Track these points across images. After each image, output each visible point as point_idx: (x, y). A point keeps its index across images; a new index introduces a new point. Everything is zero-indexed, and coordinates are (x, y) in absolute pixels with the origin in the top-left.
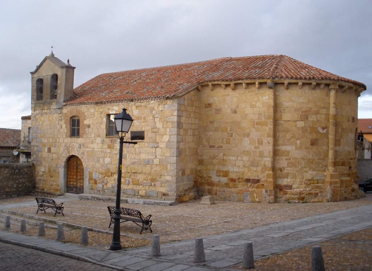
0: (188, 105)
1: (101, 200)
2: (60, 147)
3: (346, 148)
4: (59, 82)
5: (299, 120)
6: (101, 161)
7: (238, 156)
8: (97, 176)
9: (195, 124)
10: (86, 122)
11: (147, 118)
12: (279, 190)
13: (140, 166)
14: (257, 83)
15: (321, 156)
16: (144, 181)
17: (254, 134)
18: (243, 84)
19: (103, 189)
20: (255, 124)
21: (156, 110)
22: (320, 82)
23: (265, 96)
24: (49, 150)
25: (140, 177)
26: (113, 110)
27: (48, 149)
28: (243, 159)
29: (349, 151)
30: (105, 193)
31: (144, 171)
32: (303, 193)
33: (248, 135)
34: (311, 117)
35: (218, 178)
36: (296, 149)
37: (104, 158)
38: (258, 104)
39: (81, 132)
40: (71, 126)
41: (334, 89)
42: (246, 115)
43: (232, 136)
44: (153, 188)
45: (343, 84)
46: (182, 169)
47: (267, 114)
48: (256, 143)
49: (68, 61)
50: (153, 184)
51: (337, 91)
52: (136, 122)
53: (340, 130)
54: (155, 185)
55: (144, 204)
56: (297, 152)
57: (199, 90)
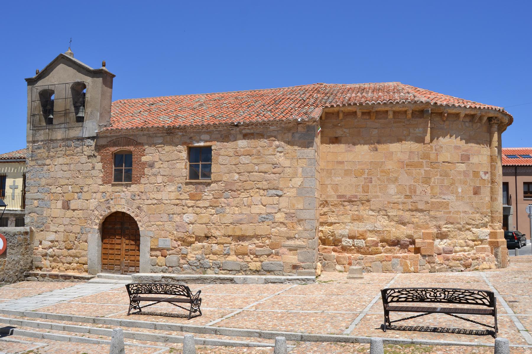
24: (66, 206)
28: (389, 214)
31: (258, 233)
35: (351, 241)
39: (135, 173)
42: (392, 153)
55: (266, 283)
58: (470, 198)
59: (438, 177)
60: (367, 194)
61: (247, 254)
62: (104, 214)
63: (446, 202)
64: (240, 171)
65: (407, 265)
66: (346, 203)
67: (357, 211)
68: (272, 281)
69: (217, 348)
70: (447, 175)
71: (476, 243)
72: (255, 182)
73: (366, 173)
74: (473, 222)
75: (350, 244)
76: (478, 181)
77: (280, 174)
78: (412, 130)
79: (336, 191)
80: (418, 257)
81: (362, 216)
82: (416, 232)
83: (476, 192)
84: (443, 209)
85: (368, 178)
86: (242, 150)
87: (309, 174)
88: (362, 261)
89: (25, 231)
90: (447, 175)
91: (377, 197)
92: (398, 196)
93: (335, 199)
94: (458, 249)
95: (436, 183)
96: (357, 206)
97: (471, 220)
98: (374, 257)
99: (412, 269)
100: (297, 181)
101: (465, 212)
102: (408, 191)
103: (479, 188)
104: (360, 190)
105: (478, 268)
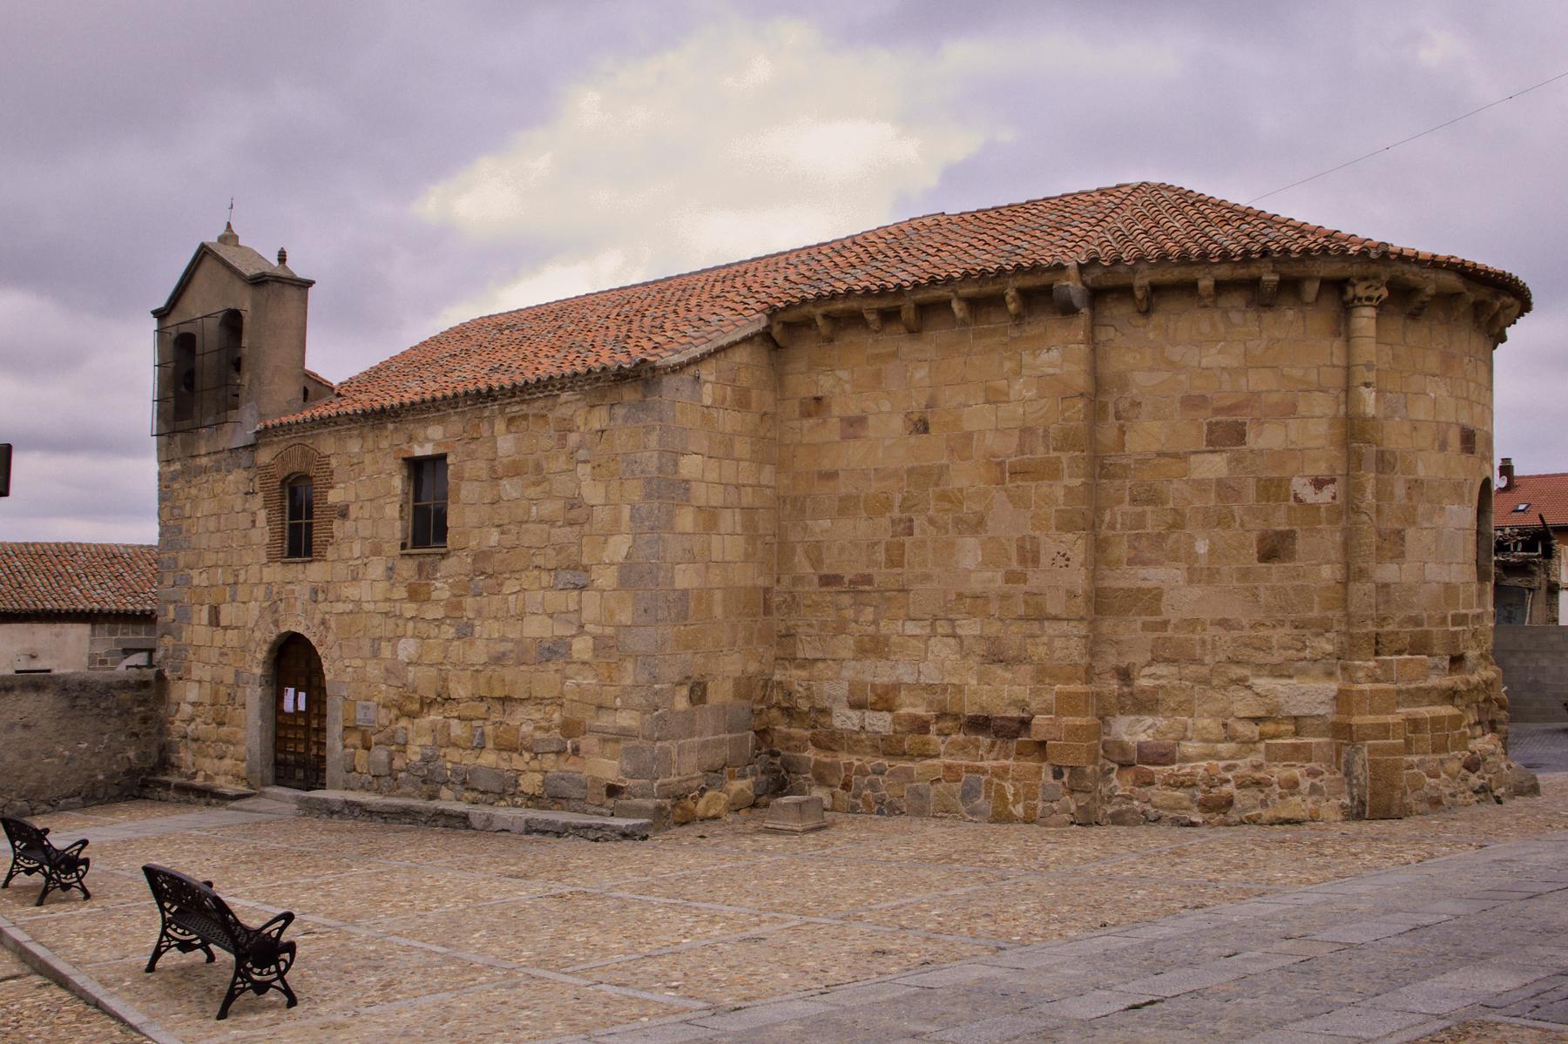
0: (720, 403)
1: (375, 817)
2: (250, 601)
3: (1433, 571)
4: (245, 341)
5: (1204, 448)
6: (386, 651)
7: (935, 619)
9: (760, 485)
10: (334, 497)
11: (548, 464)
12: (1116, 767)
13: (523, 668)
14: (1011, 293)
15: (1311, 609)
16: (539, 735)
17: (1007, 522)
18: (955, 306)
19: (391, 768)
20: (1007, 474)
21: (582, 429)
22: (1295, 271)
23: (1049, 350)
24: (215, 620)
25: (525, 721)
26: (427, 440)
27: (210, 612)
28: (959, 631)
29: (1447, 586)
30: (399, 788)
31: (538, 691)
32: (1228, 781)
34: (1258, 435)
35: (855, 715)
36: (1190, 582)
37: (394, 639)
38: (1018, 385)
39: (318, 536)
40: (287, 515)
41: (1369, 299)
42: (969, 436)
43: (911, 534)
44: (569, 766)
45: (1411, 274)
46: (688, 678)
48: (1010, 559)
49: (282, 257)
50: (572, 743)
51: (1381, 307)
52: (507, 486)
53: (1400, 491)
54: (576, 751)
56: (1197, 591)
57: (774, 341)
58: (1245, 574)
60: (899, 570)
61: (516, 750)
62: (268, 640)
63: (1150, 591)
64: (501, 522)
65: (1001, 796)
69: (525, 1001)
70: (1153, 498)
71: (1269, 728)
72: (532, 551)
74: (1260, 657)
75: (854, 725)
77: (582, 524)
78: (1027, 359)
79: (816, 562)
82: (1039, 690)
83: (1273, 549)
84: (1139, 614)
85: (901, 520)
87: (647, 523)
91: (927, 577)
94: (1190, 748)
95: (1118, 526)
97: (1250, 651)
98: (912, 769)
100: (619, 547)
101: (1224, 623)
102: (1014, 557)
103: (1289, 536)
104: (881, 556)
105: (1259, 816)
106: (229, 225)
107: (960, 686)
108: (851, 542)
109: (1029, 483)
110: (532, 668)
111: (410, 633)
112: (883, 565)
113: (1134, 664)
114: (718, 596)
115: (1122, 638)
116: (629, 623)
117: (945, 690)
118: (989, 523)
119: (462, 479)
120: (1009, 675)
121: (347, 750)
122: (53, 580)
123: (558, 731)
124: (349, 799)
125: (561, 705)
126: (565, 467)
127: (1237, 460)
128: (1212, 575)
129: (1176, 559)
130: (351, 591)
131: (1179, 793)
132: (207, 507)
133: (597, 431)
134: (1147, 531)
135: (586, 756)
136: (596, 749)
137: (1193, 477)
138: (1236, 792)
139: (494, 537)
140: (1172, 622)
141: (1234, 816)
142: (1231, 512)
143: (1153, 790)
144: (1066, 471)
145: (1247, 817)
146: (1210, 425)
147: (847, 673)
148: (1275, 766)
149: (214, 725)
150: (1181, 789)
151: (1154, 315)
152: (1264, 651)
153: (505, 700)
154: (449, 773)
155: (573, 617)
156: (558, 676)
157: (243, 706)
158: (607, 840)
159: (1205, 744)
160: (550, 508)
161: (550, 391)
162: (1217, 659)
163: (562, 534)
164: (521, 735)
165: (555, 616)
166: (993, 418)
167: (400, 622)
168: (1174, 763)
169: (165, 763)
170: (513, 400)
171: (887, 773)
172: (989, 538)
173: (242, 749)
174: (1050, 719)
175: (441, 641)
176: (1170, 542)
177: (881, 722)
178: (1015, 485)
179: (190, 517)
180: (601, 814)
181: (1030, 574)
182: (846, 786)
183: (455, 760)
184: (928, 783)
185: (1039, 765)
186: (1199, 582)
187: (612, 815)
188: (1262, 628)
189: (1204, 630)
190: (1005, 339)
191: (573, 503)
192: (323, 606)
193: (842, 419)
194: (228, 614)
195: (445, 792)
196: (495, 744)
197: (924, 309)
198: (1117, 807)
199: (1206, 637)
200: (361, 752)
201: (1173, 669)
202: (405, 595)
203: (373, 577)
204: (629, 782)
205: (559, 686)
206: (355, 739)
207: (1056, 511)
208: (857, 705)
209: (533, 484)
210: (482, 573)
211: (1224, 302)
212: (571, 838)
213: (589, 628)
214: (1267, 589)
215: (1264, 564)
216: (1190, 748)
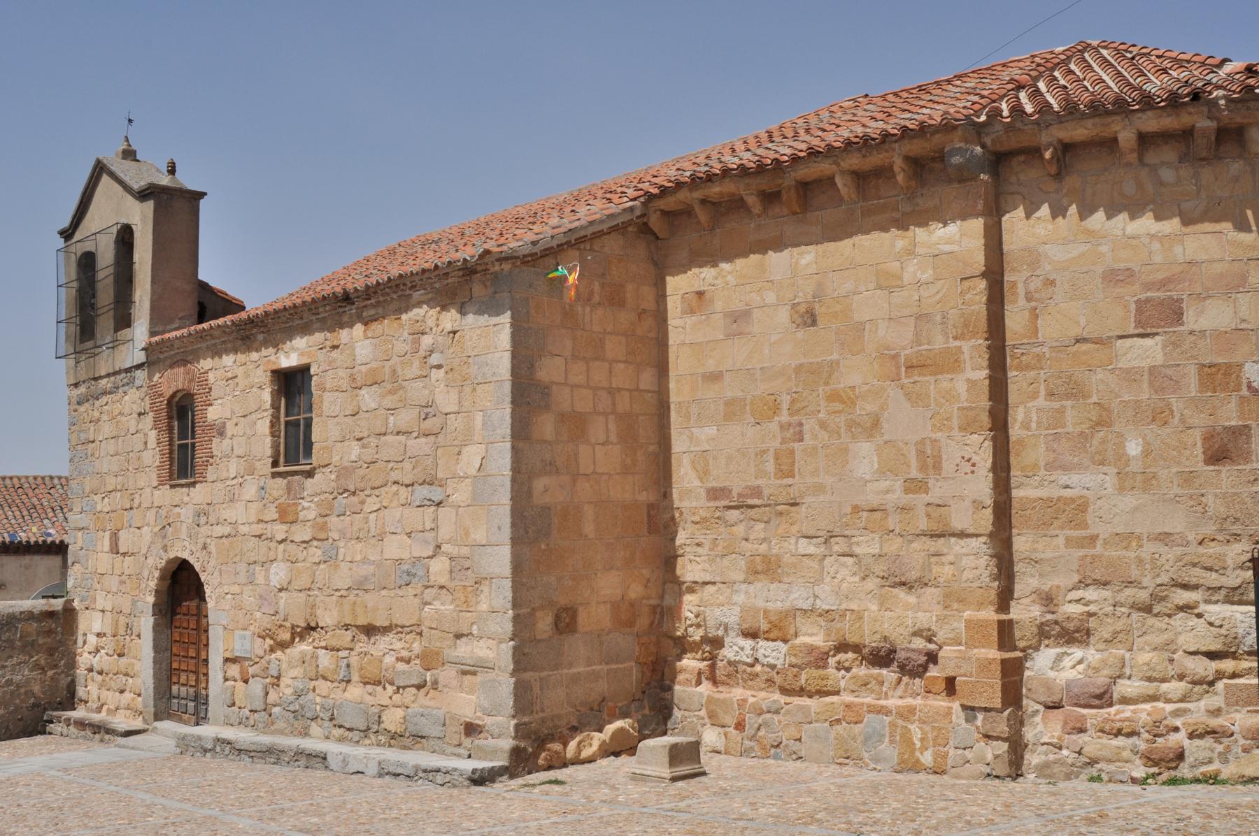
5: (1132, 331)
8: (248, 646)
12: (1041, 708)
13: (384, 592)
18: (839, 181)
20: (903, 369)
24: (115, 549)
28: (857, 550)
32: (1176, 729)
33: (874, 426)
35: (748, 643)
36: (1121, 489)
42: (860, 327)
43: (801, 440)
47: (953, 314)
56: (1129, 501)
58: (1188, 478)
59: (1041, 401)
60: (789, 481)
63: (1073, 500)
65: (907, 740)
66: (733, 515)
67: (764, 540)
68: (392, 769)
70: (1075, 391)
71: (1228, 665)
72: (391, 465)
73: (785, 406)
74: (1212, 579)
76: (1233, 404)
79: (703, 474)
80: (949, 713)
81: (779, 558)
84: (1062, 528)
85: (790, 425)
86: (363, 368)
88: (776, 718)
89: (46, 608)
90: (1075, 391)
91: (819, 489)
92: (885, 484)
93: (703, 502)
95: (1034, 425)
96: (762, 525)
98: (808, 707)
99: (927, 758)
101: (1164, 538)
102: (914, 463)
103: (1241, 432)
104: (770, 466)
106: (127, 139)
107: (859, 612)
108: (738, 450)
109: (927, 378)
110: (392, 593)
111: (280, 556)
112: (772, 475)
113: (1058, 587)
114: (589, 511)
115: (1042, 556)
116: (484, 543)
117: (843, 616)
118: (885, 425)
119: (324, 390)
120: (912, 599)
121: (228, 683)
122: (25, 513)
123: (418, 661)
124: (222, 736)
125: (420, 634)
126: (420, 373)
127: (1173, 343)
128: (1148, 481)
129: (1102, 463)
130: (230, 513)
131: (1120, 741)
132: (107, 429)
133: (449, 333)
134: (1066, 430)
135: (445, 690)
136: (454, 683)
137: (1120, 365)
138: (1186, 742)
139: (354, 450)
140: (1101, 536)
141: (1184, 771)
142: (1169, 405)
143: (1084, 738)
144: (968, 364)
145: (1202, 774)
146: (1138, 302)
147: (740, 598)
148: (1237, 711)
149: (116, 656)
150: (1120, 738)
151: (1067, 178)
152: (1216, 571)
153: (370, 630)
154: (318, 708)
155: (430, 536)
156: (417, 600)
157: (139, 636)
158: (455, 786)
159: (1147, 684)
160: (405, 418)
161: (403, 290)
162: (1159, 581)
163: (420, 445)
164: (384, 666)
165: (413, 535)
166: (886, 305)
167: (273, 545)
168: (1111, 705)
169: (69, 699)
170: (369, 302)
171: (783, 711)
172: (886, 443)
173: (139, 681)
174: (960, 651)
175: (308, 565)
176: (1095, 442)
177: (772, 652)
178: (911, 380)
179: (93, 442)
180: (459, 756)
181: (931, 483)
182: (740, 726)
183: (324, 694)
184: (827, 724)
185: (950, 705)
186: (1133, 488)
187: (469, 757)
188: (1212, 544)
189: (1141, 546)
190: (896, 215)
191: (427, 410)
192: (204, 530)
193: (727, 315)
194: (126, 540)
195: (315, 729)
196: (361, 676)
197: (806, 188)
198: (1043, 757)
199: (1143, 555)
200: (240, 684)
201: (1106, 593)
202: (276, 516)
203: (248, 498)
204: (488, 721)
205: (418, 612)
206: (234, 670)
207: (959, 408)
208: (752, 634)
209: (390, 392)
210: (346, 490)
211: (1151, 157)
212: (420, 782)
213: (445, 547)
214: (1216, 496)
215: (1212, 468)
216: (1126, 687)
